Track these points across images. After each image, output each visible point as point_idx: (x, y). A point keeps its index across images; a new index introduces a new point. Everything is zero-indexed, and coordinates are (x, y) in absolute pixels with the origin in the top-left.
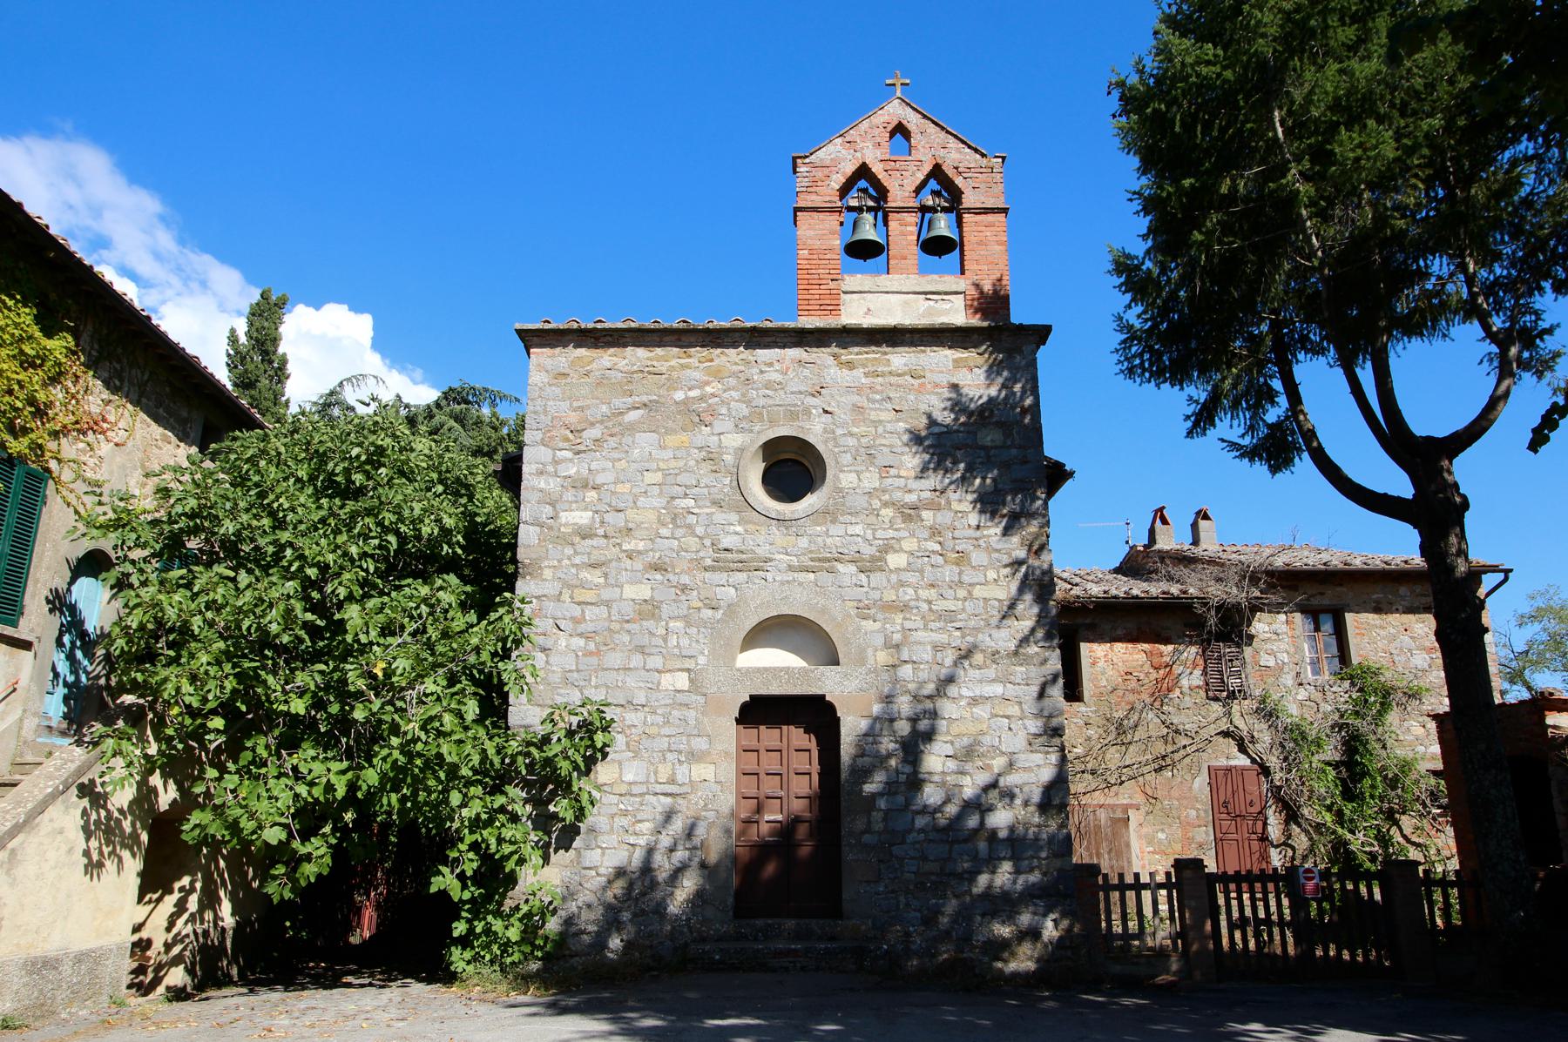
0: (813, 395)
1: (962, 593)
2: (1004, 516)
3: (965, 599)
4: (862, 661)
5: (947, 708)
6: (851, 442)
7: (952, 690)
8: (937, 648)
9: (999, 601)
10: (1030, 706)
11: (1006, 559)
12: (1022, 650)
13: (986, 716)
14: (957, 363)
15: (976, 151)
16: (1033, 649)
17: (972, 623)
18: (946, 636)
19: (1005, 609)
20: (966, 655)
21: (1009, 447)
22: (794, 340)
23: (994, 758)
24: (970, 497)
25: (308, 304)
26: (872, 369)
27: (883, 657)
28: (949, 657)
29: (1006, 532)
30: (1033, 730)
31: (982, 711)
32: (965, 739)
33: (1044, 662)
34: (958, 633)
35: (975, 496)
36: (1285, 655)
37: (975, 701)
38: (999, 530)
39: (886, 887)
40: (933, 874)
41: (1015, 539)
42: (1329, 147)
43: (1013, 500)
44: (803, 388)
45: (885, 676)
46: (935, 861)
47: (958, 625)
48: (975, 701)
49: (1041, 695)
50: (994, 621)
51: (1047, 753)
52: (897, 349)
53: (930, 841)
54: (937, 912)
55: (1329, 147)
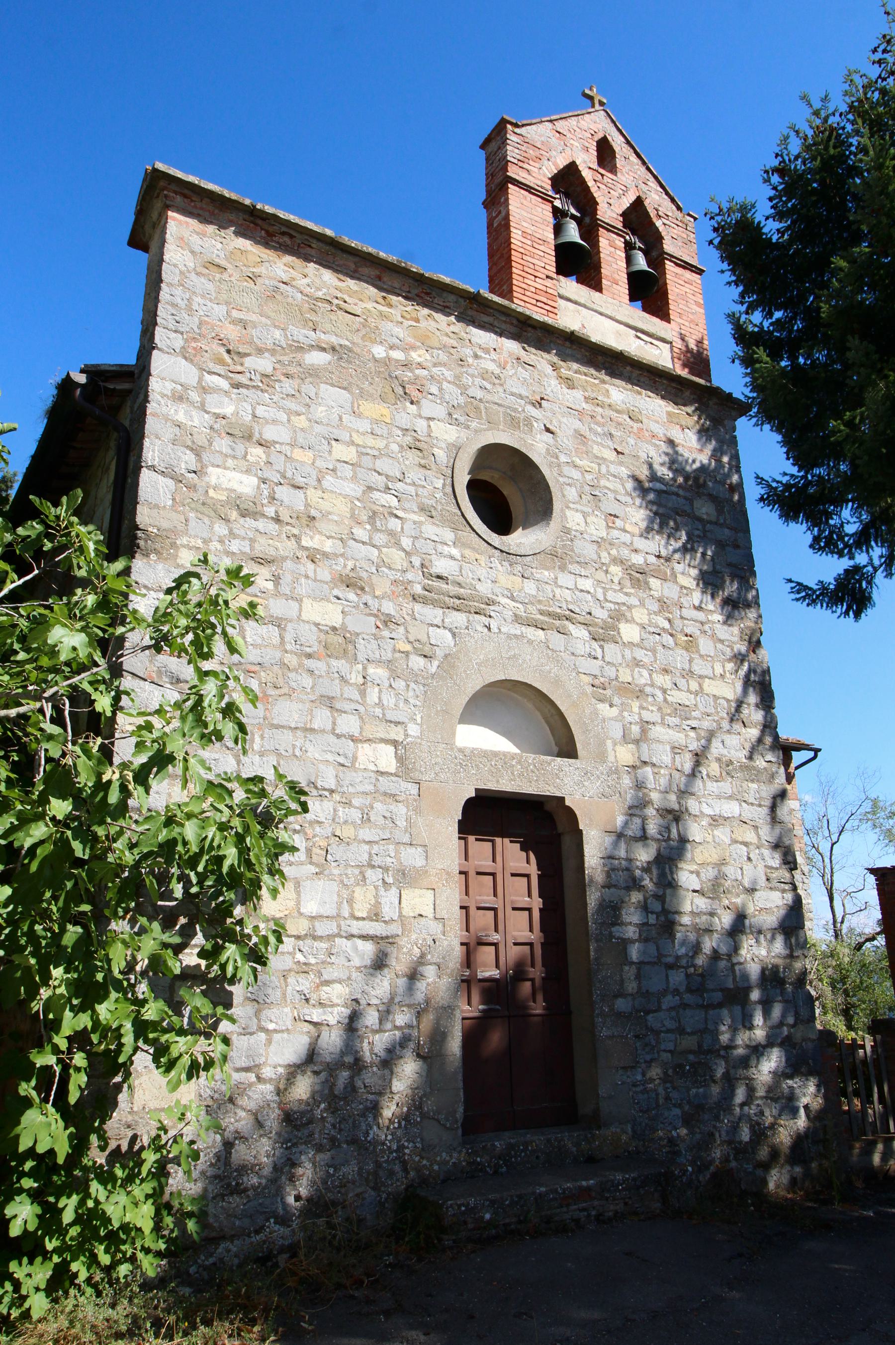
22: (513, 330)
40: (691, 1052)
46: (693, 1033)
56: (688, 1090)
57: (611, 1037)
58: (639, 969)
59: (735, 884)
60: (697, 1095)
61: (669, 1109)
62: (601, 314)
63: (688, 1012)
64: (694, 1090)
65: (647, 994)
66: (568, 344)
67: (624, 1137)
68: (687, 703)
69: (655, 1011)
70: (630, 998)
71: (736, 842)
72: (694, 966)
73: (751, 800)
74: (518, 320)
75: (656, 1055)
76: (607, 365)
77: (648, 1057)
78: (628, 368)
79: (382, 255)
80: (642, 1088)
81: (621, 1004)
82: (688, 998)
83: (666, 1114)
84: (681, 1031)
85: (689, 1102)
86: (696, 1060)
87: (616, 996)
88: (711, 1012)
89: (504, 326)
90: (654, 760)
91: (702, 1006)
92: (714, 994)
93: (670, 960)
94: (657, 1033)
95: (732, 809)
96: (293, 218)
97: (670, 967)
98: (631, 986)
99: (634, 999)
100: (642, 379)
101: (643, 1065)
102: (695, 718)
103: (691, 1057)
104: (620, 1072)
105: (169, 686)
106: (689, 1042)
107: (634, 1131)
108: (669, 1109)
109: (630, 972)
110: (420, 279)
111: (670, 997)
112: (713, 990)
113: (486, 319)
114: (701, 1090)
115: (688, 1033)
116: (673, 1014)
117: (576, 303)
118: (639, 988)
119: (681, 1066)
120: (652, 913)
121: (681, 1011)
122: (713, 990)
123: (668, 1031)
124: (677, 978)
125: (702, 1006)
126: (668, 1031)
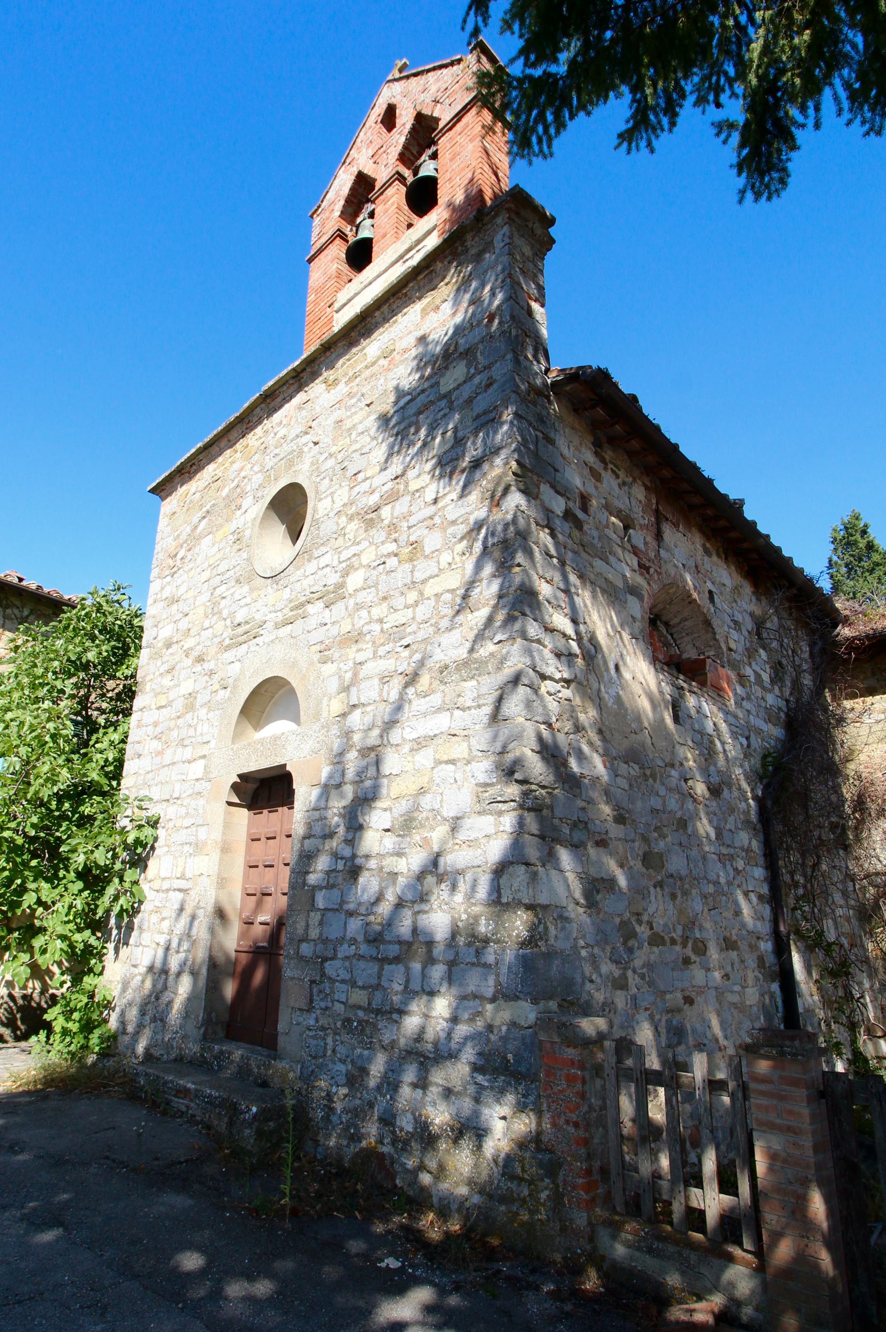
0: (306, 433)
1: (412, 596)
2: (463, 471)
3: (417, 603)
4: (317, 715)
5: (392, 763)
6: (331, 463)
7: (395, 736)
8: (385, 679)
9: (452, 591)
10: (481, 738)
11: (462, 529)
12: (475, 655)
13: (429, 764)
14: (424, 312)
15: (452, 64)
16: (488, 648)
17: (421, 635)
18: (392, 661)
19: (458, 600)
20: (412, 679)
21: (473, 376)
22: (296, 386)
23: (433, 829)
24: (429, 466)
25: (742, 513)
26: (351, 374)
27: (337, 706)
28: (396, 684)
29: (464, 492)
30: (482, 778)
31: (425, 758)
32: (404, 802)
33: (503, 660)
34: (406, 653)
35: (434, 461)
36: (405, 510)
37: (419, 744)
38: (454, 495)
39: (317, 1020)
40: (360, 1007)
41: (474, 496)
42: (794, 112)
43: (474, 443)
44: (298, 431)
45: (335, 730)
46: (363, 988)
47: (405, 642)
48: (419, 744)
49: (495, 717)
50: (445, 623)
51: (500, 813)
52: (373, 337)
53: (362, 957)
54: (364, 1071)
55: (794, 112)
56: (354, 1049)
57: (292, 979)
58: (323, 915)
59: (430, 815)
60: (361, 1056)
61: (334, 1063)
62: (370, 283)
63: (362, 964)
64: (359, 1050)
65: (325, 941)
66: (328, 354)
67: (291, 1075)
68: (404, 621)
69: (332, 959)
70: (312, 943)
71: (441, 763)
72: (374, 914)
73: (469, 703)
74: (293, 378)
75: (330, 1004)
76: (363, 331)
77: (323, 1005)
78: (377, 314)
79: (220, 428)
80: (314, 1033)
81: (306, 949)
82: (364, 949)
83: (330, 1066)
84: (353, 984)
85: (352, 1061)
86: (366, 1018)
87: (301, 941)
88: (386, 967)
89: (290, 391)
90: (362, 700)
91: (376, 959)
92: (391, 947)
93: (351, 906)
94: (332, 981)
95: (442, 722)
96: (186, 457)
97: (351, 914)
98: (314, 933)
99: (316, 945)
100: (394, 306)
101: (318, 1012)
102: (410, 634)
103: (361, 1013)
104: (298, 1013)
105: (745, 633)
106: (359, 997)
107: (301, 1073)
108: (334, 1063)
109: (315, 917)
110: (240, 420)
111: (345, 946)
112: (390, 942)
113: (279, 399)
114: (366, 1052)
115: (359, 987)
116: (347, 964)
117: (356, 294)
118: (321, 934)
119: (348, 1020)
120: (342, 858)
121: (354, 961)
122: (390, 942)
123: (343, 981)
124: (354, 926)
125: (376, 959)
126: (343, 981)
